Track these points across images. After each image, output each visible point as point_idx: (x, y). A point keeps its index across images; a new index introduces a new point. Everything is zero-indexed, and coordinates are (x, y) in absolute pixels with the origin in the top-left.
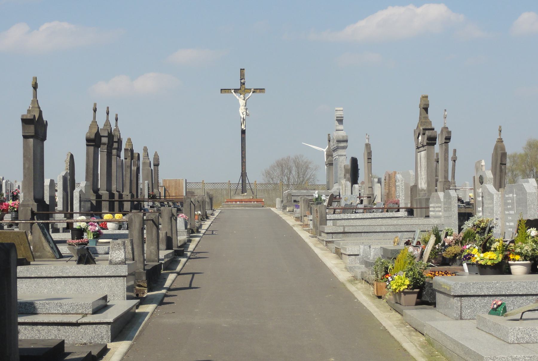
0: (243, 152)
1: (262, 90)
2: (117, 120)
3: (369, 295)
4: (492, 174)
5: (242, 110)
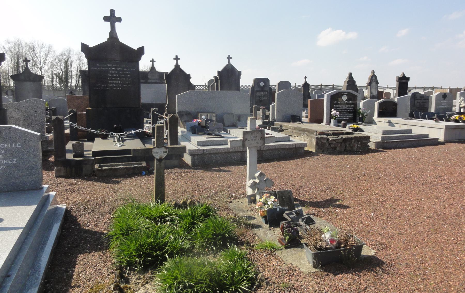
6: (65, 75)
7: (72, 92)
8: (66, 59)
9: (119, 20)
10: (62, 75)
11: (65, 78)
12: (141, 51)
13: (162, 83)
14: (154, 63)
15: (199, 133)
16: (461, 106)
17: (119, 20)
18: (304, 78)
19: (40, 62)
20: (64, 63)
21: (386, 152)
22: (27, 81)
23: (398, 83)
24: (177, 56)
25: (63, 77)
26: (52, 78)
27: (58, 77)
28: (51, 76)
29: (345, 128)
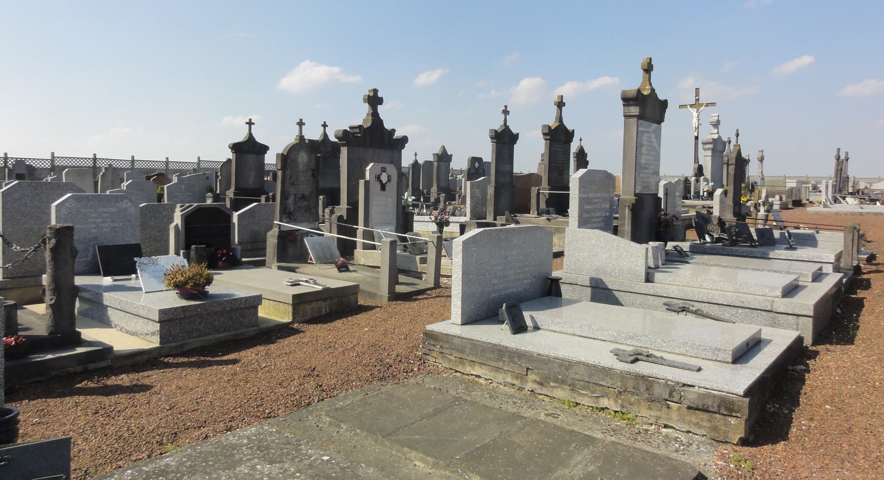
0: (696, 154)
1: (713, 104)
2: (737, 135)
3: (664, 311)
4: (577, 221)
5: (695, 120)
9: (254, 124)
12: (404, 140)
13: (695, 162)
14: (252, 126)
16: (704, 190)
17: (254, 124)
18: (323, 125)
21: (221, 274)
22: (251, 153)
23: (576, 162)
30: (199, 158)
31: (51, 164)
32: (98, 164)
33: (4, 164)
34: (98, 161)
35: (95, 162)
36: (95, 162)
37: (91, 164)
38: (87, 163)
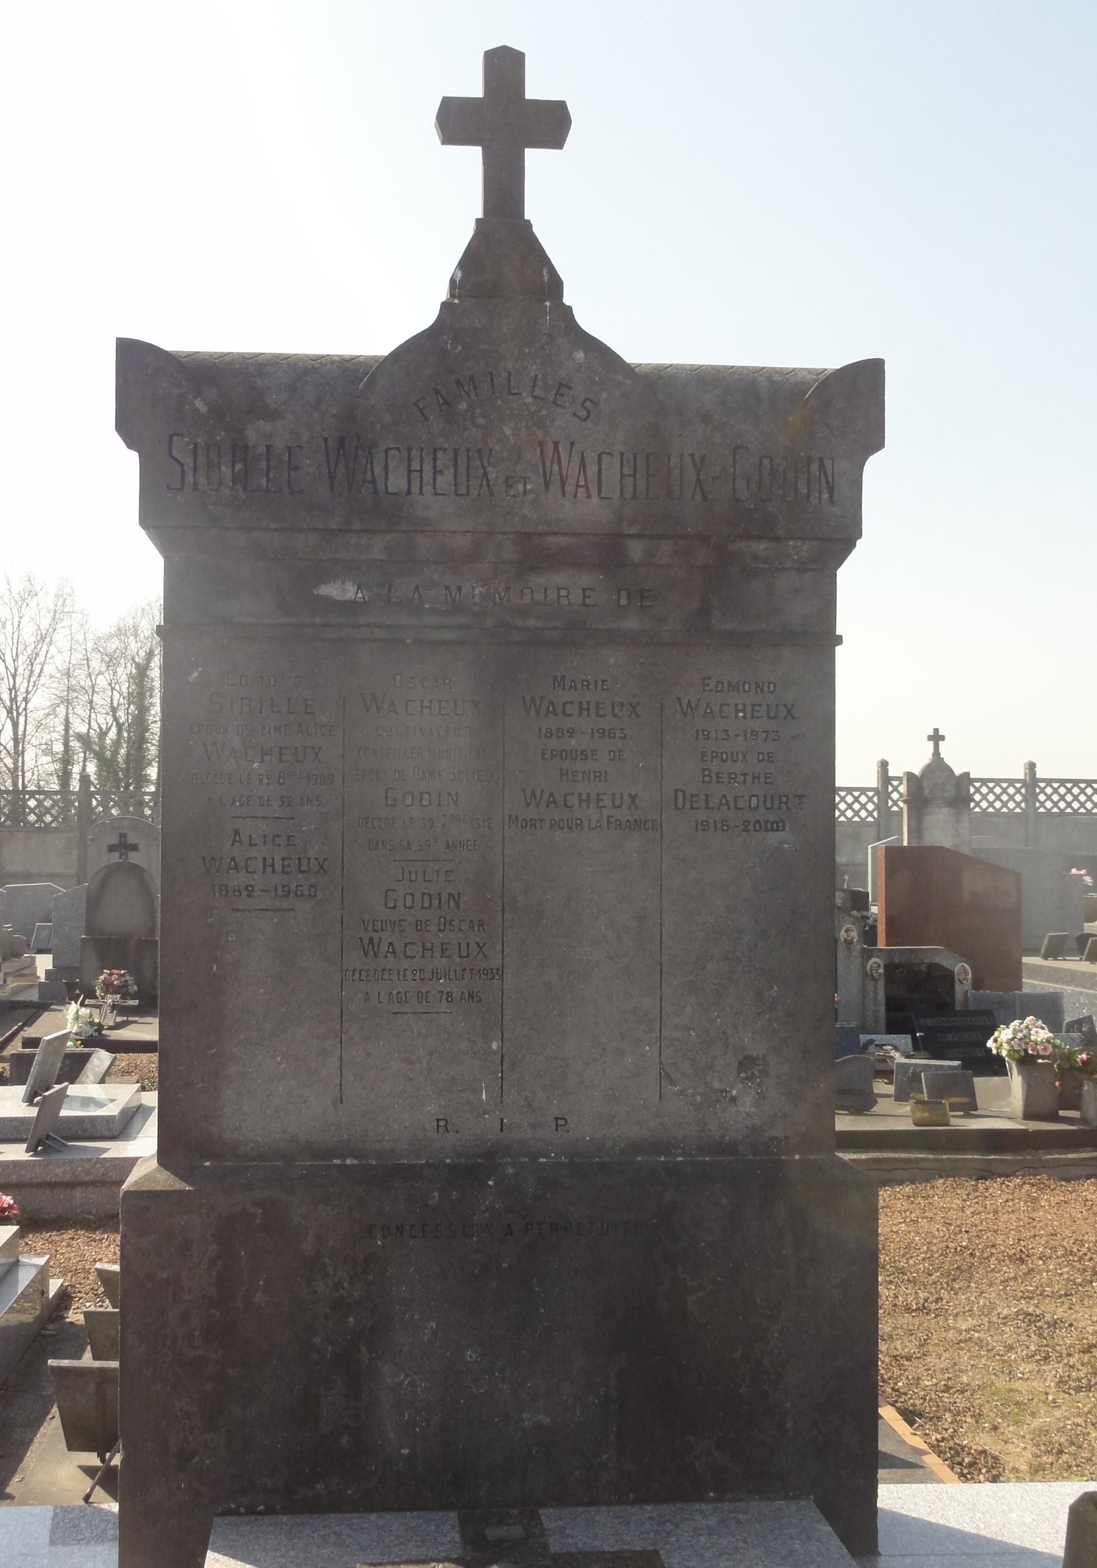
6: (128, 742)
7: (132, 839)
8: (142, 654)
10: (117, 744)
11: (127, 761)
15: (1061, 1113)
19: (14, 676)
20: (130, 676)
21: (61, 1010)
24: (936, 731)
25: (123, 751)
26: (66, 760)
27: (94, 751)
28: (58, 747)
29: (80, 1358)
30: (884, 765)
31: (877, 807)
32: (843, 813)
33: (875, 814)
34: (978, 790)
35: (1031, 797)
36: (1031, 797)
37: (870, 814)
38: (991, 797)
